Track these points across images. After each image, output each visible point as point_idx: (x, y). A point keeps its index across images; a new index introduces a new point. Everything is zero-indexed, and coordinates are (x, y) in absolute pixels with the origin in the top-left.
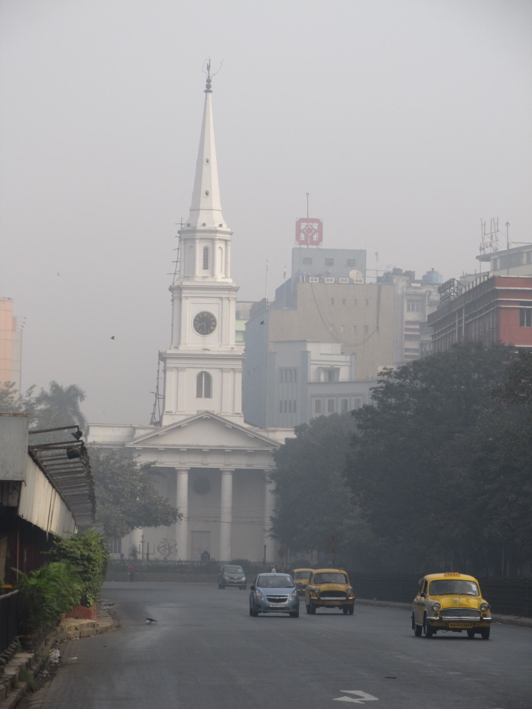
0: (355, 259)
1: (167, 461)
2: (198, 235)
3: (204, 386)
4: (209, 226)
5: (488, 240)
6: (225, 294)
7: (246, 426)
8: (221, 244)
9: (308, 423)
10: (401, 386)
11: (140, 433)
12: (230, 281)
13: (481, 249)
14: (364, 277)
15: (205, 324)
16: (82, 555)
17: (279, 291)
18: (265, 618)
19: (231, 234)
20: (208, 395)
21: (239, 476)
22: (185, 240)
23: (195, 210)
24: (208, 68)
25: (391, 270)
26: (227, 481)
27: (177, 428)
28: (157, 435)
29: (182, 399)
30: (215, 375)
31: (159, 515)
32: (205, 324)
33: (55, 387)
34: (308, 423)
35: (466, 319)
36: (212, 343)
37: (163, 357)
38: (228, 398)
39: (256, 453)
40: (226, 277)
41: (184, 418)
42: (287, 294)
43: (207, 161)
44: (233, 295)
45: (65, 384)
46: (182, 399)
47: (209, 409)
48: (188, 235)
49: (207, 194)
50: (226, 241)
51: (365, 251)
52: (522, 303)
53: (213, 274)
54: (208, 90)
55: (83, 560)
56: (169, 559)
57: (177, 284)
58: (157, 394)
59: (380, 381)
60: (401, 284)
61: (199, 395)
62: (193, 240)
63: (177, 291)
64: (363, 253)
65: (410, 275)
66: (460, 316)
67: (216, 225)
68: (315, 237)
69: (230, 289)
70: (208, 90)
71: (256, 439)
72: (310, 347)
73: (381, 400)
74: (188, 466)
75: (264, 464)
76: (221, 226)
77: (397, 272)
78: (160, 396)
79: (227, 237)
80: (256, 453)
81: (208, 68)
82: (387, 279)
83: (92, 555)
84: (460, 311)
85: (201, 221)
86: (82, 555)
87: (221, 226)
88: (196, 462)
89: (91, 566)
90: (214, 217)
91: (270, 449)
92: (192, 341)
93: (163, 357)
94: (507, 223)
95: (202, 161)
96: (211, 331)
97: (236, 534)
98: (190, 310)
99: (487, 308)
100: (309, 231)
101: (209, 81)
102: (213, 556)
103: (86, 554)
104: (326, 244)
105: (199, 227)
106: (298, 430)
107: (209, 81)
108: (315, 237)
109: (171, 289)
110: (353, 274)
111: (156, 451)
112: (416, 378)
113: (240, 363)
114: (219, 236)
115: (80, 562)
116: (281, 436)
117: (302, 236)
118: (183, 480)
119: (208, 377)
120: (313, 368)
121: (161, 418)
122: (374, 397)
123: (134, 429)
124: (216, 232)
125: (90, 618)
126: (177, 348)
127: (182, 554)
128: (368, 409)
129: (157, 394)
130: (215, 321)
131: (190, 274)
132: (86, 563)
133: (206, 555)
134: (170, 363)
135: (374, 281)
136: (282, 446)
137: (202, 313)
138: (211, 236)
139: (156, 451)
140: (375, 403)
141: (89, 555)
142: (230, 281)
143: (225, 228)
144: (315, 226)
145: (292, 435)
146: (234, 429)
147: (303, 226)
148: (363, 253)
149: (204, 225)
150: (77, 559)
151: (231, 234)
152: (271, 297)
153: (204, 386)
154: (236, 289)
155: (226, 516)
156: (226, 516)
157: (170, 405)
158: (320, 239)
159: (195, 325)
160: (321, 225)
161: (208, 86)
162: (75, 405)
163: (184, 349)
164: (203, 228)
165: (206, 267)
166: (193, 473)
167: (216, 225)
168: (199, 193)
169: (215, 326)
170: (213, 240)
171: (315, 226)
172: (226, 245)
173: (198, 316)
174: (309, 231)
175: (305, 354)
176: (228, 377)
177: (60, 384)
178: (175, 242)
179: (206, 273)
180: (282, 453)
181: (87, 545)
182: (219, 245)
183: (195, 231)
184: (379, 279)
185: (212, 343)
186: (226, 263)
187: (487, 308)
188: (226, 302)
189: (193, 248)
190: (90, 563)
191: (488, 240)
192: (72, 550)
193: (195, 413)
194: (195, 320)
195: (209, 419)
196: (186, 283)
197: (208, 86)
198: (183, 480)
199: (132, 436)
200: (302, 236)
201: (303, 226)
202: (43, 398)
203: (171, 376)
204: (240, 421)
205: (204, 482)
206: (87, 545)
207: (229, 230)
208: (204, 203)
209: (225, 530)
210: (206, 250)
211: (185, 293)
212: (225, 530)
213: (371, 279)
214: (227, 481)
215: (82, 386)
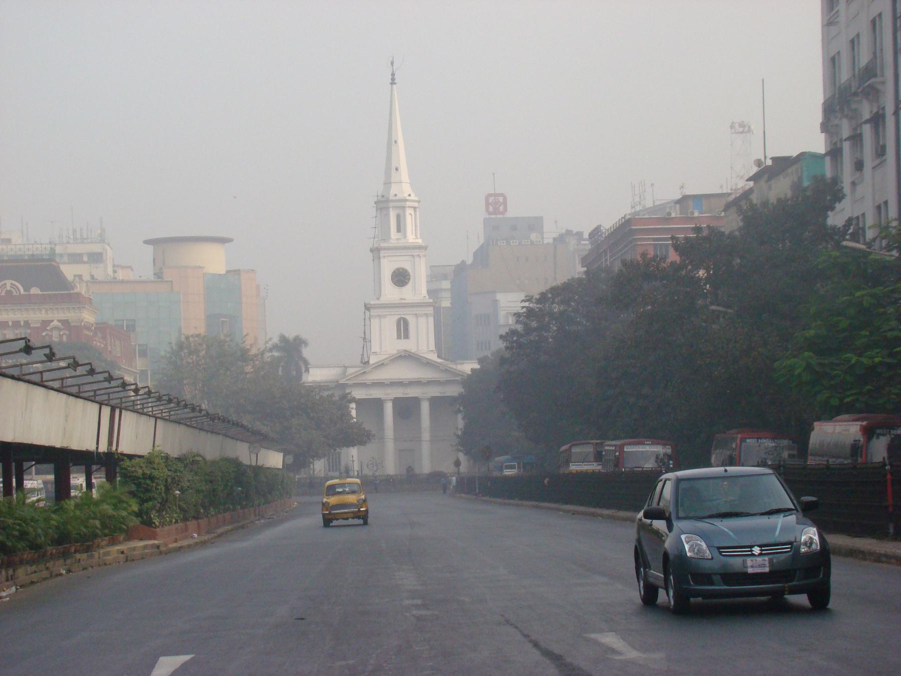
0: (535, 224)
1: (376, 393)
2: (391, 204)
3: (403, 329)
4: (400, 196)
5: (637, 199)
6: (416, 252)
7: (439, 360)
8: (411, 211)
9: (489, 355)
10: (540, 310)
11: (350, 371)
12: (420, 241)
13: (632, 208)
14: (543, 238)
15: (401, 278)
16: (144, 474)
17: (476, 254)
18: (342, 529)
19: (419, 202)
20: (407, 336)
21: (435, 402)
22: (381, 209)
23: (388, 183)
24: (392, 63)
25: (564, 231)
26: (425, 407)
27: (381, 365)
28: (365, 372)
29: (385, 341)
30: (411, 320)
31: (357, 437)
32: (401, 278)
33: (283, 339)
34: (489, 355)
35: (611, 257)
36: (407, 294)
37: (367, 307)
38: (423, 339)
39: (448, 382)
40: (417, 238)
41: (385, 357)
42: (482, 255)
43: (396, 142)
44: (422, 253)
45: (291, 335)
46: (385, 341)
47: (408, 349)
48: (383, 204)
49: (397, 169)
50: (415, 208)
51: (542, 218)
52: (655, 240)
53: (405, 237)
54: (393, 82)
55: (145, 478)
56: (377, 474)
57: (375, 246)
58: (364, 338)
59: (523, 307)
60: (572, 243)
61: (399, 337)
62: (387, 208)
63: (376, 251)
64: (540, 220)
65: (579, 235)
66: (606, 255)
67: (406, 195)
68: (501, 208)
69: (419, 248)
70: (393, 82)
71: (447, 371)
72: (500, 296)
73: (525, 324)
74: (392, 396)
75: (454, 391)
76: (409, 195)
77: (569, 233)
78: (366, 340)
79: (416, 205)
80: (448, 382)
81: (392, 63)
82: (561, 239)
83: (155, 473)
84: (605, 251)
85: (392, 192)
86: (144, 474)
87: (409, 195)
88: (399, 393)
89: (154, 485)
90: (404, 188)
91: (459, 378)
92: (390, 293)
93: (367, 307)
94: (652, 184)
95: (391, 143)
96: (406, 283)
97: (434, 450)
98: (388, 267)
99: (626, 246)
100: (495, 203)
101: (393, 75)
102: (417, 471)
103: (148, 472)
104: (512, 212)
105: (392, 197)
106: (481, 361)
107: (393, 75)
108: (501, 208)
109: (371, 250)
110: (534, 236)
111: (364, 385)
112: (553, 303)
113: (432, 308)
114: (408, 204)
115: (143, 481)
116: (468, 367)
117: (491, 209)
118: (389, 408)
119: (406, 322)
120: (502, 314)
121: (369, 358)
122: (517, 322)
123: (346, 367)
124: (406, 200)
125: (155, 539)
126: (378, 299)
127: (391, 467)
128: (513, 332)
129: (364, 338)
130: (409, 275)
131: (386, 237)
132: (148, 482)
133: (410, 469)
134: (374, 312)
135: (551, 241)
136: (468, 375)
137: (398, 269)
138: (401, 205)
139: (364, 385)
140: (520, 328)
141: (151, 474)
142: (420, 241)
143: (413, 197)
144: (501, 199)
145: (477, 366)
146: (429, 364)
147: (491, 199)
148: (540, 220)
149: (396, 195)
150: (139, 478)
151: (419, 202)
152: (469, 261)
153: (403, 329)
154: (425, 248)
155: (426, 435)
156: (426, 435)
157: (375, 347)
158: (505, 210)
159: (392, 279)
160: (505, 199)
161: (393, 79)
162: (300, 352)
163: (384, 300)
164: (394, 198)
165: (399, 230)
166: (397, 402)
167: (406, 195)
168: (390, 169)
169: (409, 279)
170: (404, 208)
171: (501, 199)
172: (415, 211)
173: (394, 272)
174: (495, 203)
175: (495, 302)
176: (422, 320)
177: (287, 335)
178: (373, 212)
179: (399, 235)
180: (470, 381)
181: (150, 463)
182: (409, 211)
183: (388, 201)
184: (555, 239)
185: (407, 294)
186: (416, 226)
187: (626, 246)
188: (417, 259)
189: (387, 215)
190: (153, 482)
191: (637, 199)
192: (133, 469)
193: (395, 352)
194: (392, 276)
195: (407, 357)
196: (383, 245)
197: (393, 79)
198: (389, 408)
199: (344, 373)
200: (491, 209)
201: (491, 199)
202: (275, 347)
203: (375, 323)
204: (434, 357)
205: (406, 409)
206: (150, 463)
207: (417, 199)
208: (394, 177)
209: (426, 448)
210: (398, 216)
211: (382, 253)
212: (426, 448)
213: (548, 238)
214: (425, 407)
215: (304, 336)
